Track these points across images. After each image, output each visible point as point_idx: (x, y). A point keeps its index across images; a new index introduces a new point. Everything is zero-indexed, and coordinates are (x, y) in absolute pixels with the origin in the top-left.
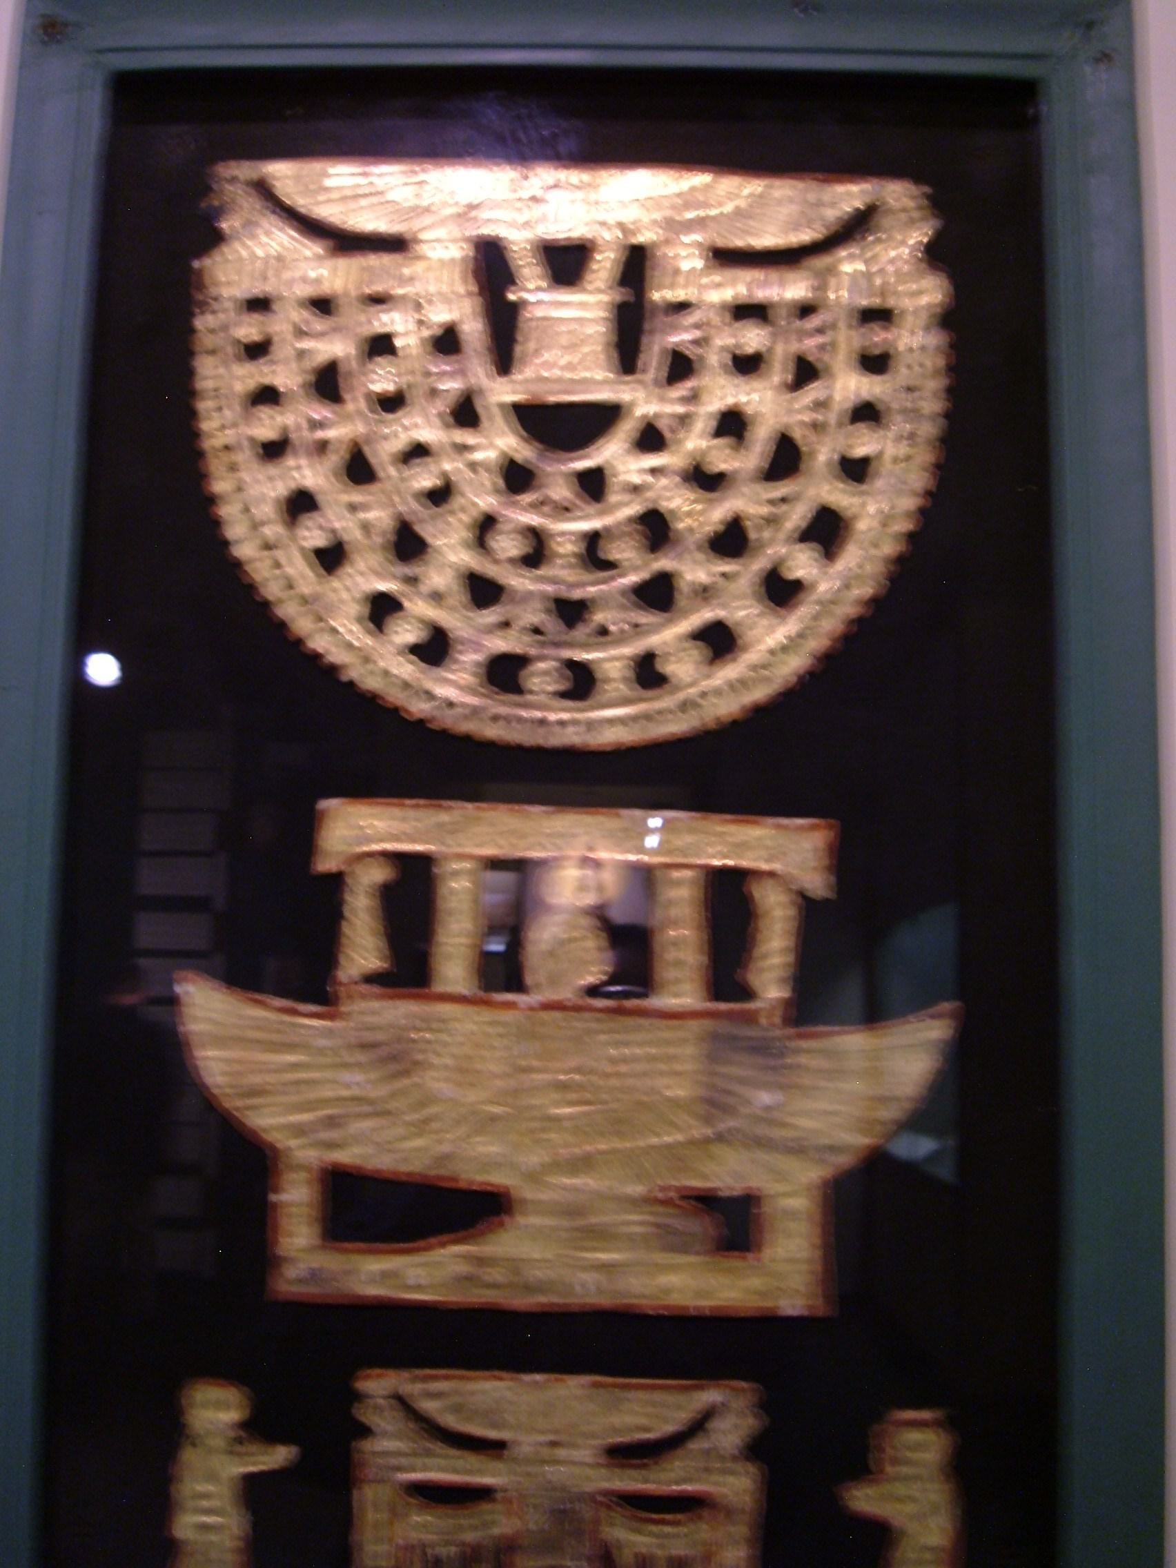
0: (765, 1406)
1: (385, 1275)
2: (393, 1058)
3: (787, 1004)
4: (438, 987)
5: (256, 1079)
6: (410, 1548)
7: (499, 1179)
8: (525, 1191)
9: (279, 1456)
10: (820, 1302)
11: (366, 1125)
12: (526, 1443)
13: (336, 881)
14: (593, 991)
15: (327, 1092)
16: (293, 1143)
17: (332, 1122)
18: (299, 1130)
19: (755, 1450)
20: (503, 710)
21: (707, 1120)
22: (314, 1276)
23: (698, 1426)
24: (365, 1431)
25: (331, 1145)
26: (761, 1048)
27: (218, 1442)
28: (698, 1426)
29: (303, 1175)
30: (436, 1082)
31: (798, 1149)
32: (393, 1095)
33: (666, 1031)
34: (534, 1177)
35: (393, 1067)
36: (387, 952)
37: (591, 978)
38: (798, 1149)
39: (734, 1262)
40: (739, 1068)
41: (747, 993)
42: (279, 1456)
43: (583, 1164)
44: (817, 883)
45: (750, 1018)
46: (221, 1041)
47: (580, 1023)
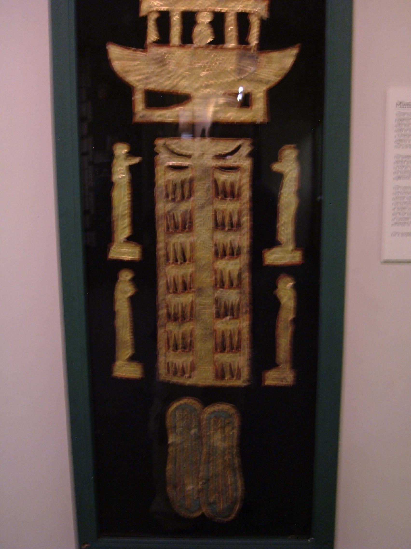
0: (253, 144)
1: (160, 116)
2: (161, 62)
3: (258, 45)
4: (171, 44)
5: (127, 69)
6: (169, 181)
7: (187, 91)
8: (194, 94)
9: (136, 160)
10: (266, 118)
11: (155, 79)
12: (196, 154)
13: (145, 19)
14: (211, 43)
15: (145, 71)
16: (137, 84)
17: (147, 78)
18: (139, 81)
19: (251, 155)
20: (135, 55)
21: (239, 74)
22: (143, 116)
23: (237, 149)
24: (157, 154)
25: (147, 84)
26: (252, 57)
27: (123, 157)
28: (237, 149)
29: (140, 91)
30: (171, 67)
31: (260, 81)
32: (162, 71)
33: (229, 53)
34: (197, 89)
35: (161, 64)
36: (159, 35)
37: (210, 40)
38: (260, 81)
39: (245, 109)
40: (246, 62)
41: (247, 43)
42: (136, 160)
43: (207, 87)
44: (264, 14)
45: (250, 49)
46: (119, 59)
47: (207, 52)
